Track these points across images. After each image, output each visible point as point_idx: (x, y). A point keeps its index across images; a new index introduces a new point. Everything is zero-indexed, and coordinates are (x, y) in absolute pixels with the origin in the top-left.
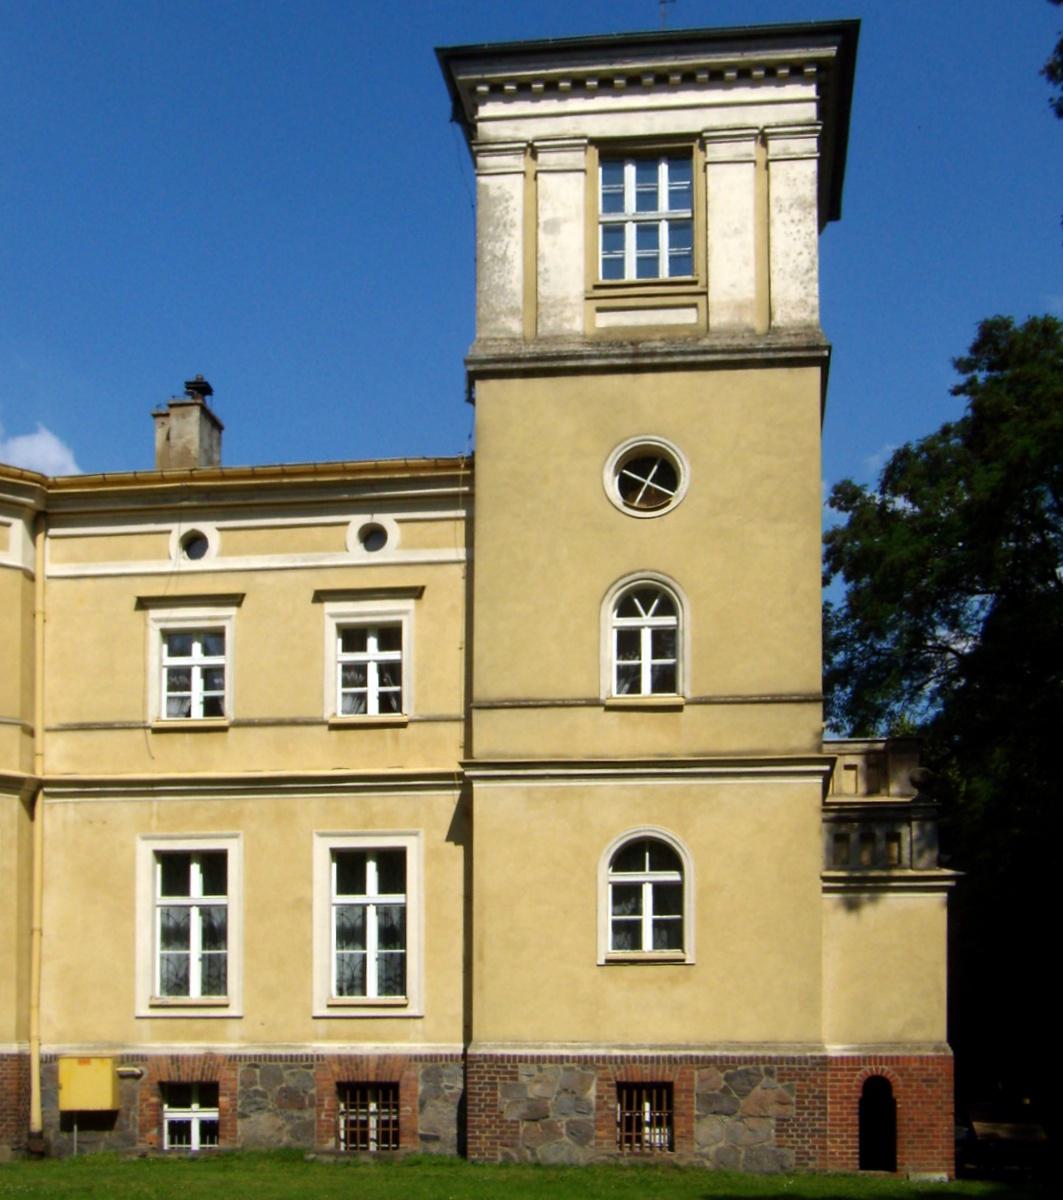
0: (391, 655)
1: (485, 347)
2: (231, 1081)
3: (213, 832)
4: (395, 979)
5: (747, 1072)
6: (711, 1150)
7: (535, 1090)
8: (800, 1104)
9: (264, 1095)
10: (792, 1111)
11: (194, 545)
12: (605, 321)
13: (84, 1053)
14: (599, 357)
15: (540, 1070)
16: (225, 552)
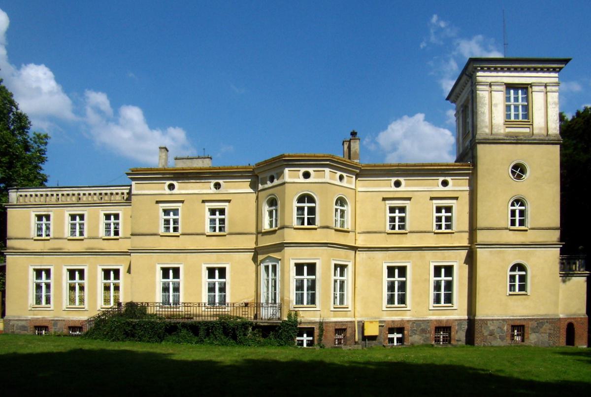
0: (222, 217)
1: (480, 136)
2: (408, 327)
3: (404, 261)
4: (449, 299)
5: (542, 322)
6: (533, 342)
7: (491, 328)
8: (554, 330)
9: (416, 331)
10: (552, 331)
11: (171, 187)
12: (508, 130)
13: (372, 320)
14: (508, 140)
15: (493, 322)
16: (179, 189)
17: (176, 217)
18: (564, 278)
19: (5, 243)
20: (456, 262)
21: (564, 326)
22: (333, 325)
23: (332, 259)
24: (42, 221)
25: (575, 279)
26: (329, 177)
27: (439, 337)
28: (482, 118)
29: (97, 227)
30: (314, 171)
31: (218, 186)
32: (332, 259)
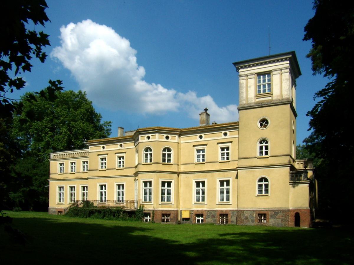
2: (205, 214)
3: (203, 178)
6: (272, 224)
7: (246, 215)
8: (285, 217)
9: (209, 216)
12: (258, 100)
16: (205, 138)
17: (228, 151)
18: (294, 185)
19: (49, 176)
20: (231, 178)
21: (293, 214)
22: (161, 212)
23: (160, 178)
24: (224, 151)
25: (300, 186)
26: (158, 138)
27: (223, 220)
28: (242, 95)
29: (68, 169)
30: (152, 135)
31: (121, 145)
32: (160, 178)
